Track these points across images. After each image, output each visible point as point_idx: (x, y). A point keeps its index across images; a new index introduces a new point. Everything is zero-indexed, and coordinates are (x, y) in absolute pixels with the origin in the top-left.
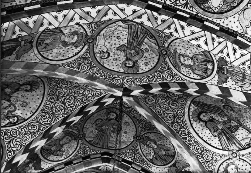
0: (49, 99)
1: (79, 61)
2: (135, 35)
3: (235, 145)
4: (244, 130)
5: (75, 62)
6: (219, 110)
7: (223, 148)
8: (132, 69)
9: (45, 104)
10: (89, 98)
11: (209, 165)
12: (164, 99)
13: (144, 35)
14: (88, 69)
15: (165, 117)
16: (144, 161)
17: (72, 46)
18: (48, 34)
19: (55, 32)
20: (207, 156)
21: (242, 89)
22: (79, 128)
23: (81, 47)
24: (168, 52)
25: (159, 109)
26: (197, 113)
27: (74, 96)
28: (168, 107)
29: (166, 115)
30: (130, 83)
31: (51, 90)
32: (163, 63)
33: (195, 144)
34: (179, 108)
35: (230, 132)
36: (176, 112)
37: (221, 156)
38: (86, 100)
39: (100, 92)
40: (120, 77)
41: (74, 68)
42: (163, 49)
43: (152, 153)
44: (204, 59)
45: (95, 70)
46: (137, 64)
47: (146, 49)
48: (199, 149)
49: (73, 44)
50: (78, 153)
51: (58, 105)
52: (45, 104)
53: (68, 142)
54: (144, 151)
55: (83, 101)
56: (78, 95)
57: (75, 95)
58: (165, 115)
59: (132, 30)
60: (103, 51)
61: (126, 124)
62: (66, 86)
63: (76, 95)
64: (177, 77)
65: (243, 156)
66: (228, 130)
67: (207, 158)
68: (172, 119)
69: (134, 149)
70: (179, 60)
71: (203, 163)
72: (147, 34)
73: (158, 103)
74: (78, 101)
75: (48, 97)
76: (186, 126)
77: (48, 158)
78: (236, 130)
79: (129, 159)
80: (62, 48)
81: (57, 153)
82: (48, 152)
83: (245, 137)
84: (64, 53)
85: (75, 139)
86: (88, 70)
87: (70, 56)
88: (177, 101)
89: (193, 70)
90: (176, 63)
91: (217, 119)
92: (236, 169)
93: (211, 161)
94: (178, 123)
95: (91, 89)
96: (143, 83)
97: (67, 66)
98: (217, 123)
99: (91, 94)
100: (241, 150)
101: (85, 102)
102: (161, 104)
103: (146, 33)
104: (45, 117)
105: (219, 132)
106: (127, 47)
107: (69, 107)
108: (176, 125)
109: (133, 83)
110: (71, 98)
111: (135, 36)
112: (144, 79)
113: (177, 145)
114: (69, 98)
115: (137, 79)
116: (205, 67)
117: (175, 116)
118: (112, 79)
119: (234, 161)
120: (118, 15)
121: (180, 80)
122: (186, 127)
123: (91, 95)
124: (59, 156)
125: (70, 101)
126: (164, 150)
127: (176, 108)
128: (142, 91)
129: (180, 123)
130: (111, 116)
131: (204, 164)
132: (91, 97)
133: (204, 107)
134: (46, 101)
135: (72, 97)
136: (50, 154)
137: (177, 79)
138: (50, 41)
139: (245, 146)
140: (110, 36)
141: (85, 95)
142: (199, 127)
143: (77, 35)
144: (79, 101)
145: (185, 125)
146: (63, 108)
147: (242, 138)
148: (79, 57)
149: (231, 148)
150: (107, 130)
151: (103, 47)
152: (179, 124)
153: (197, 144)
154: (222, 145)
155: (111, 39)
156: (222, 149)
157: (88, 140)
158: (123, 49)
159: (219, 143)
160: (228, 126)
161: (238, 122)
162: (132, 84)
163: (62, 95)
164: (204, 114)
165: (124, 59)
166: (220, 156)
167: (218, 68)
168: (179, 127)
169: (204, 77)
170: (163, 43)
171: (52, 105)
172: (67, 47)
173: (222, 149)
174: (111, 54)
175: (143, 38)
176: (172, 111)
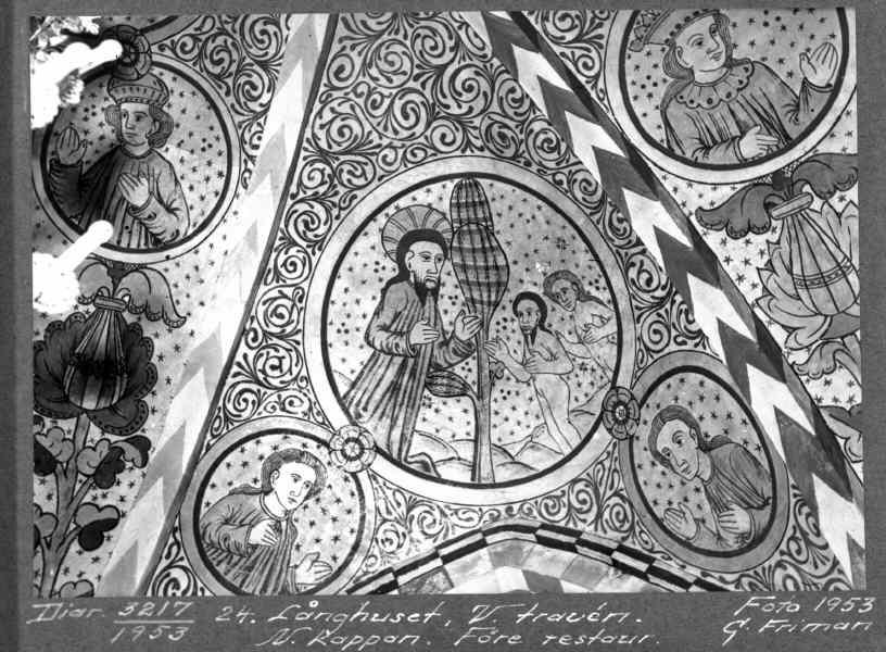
3: (392, 428)
4: (471, 417)
6: (493, 289)
7: (345, 397)
11: (246, 395)
12: (416, 62)
15: (332, 110)
20: (276, 362)
21: (763, 303)
26: (424, 224)
29: (345, 108)
33: (288, 291)
35: (423, 377)
36: (377, 142)
37: (315, 411)
44: (772, 106)
48: (281, 316)
58: (339, 105)
64: (594, 54)
65: (373, 477)
66: (425, 370)
67: (269, 371)
68: (339, 144)
70: (682, 22)
71: (239, 365)
76: (343, 214)
78: (448, 395)
83: (445, 435)
89: (674, 96)
91: (444, 304)
92: (305, 492)
93: (269, 392)
94: (336, 174)
98: (427, 315)
100: (388, 457)
105: (397, 345)
108: (323, 174)
117: (358, 147)
119: (329, 463)
121: (592, 73)
122: (337, 217)
127: (396, 132)
131: (238, 374)
133: (470, 232)
137: (583, 60)
139: (409, 460)
142: (365, 265)
145: (341, 209)
147: (433, 432)
149: (368, 422)
152: (332, 181)
153: (293, 300)
154: (353, 385)
156: (342, 395)
159: (352, 372)
160: (441, 361)
161: (486, 381)
164: (434, 249)
166: (310, 409)
167: (777, 174)
168: (322, 190)
169: (678, 152)
173: (342, 395)
176: (375, 122)
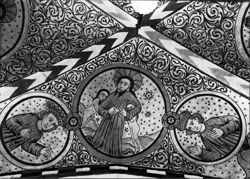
0: (29, 41)
9: (22, 48)
10: (88, 41)
15: (208, 56)
16: (188, 163)
22: (72, 100)
25: (196, 47)
27: (66, 39)
28: (208, 41)
29: (209, 53)
31: (33, 25)
34: (227, 40)
36: (223, 47)
38: (85, 43)
39: (105, 32)
43: (198, 144)
50: (67, 158)
51: (42, 52)
52: (22, 48)
53: (52, 129)
54: (184, 144)
55: (79, 46)
57: (68, 37)
61: (147, 95)
62: (56, 18)
68: (220, 58)
69: (166, 146)
74: (72, 46)
75: (27, 38)
77: (12, 152)
79: (159, 166)
81: (30, 147)
82: (15, 137)
85: (64, 127)
88: (220, 27)
95: (93, 26)
99: (93, 36)
101: (83, 46)
102: (198, 38)
104: (19, 65)
107: (58, 54)
110: (61, 42)
113: (241, 85)
114: (60, 41)
122: (246, 66)
123: (92, 38)
124: (33, 154)
125: (60, 46)
126: (219, 126)
127: (221, 40)
128: (168, 5)
129: (235, 61)
130: (123, 85)
132: (92, 39)
134: (24, 44)
135: (64, 40)
136: (17, 144)
141: (83, 36)
144: (74, 46)
145: (243, 64)
146: (49, 55)
150: (117, 116)
152: (232, 64)
157: (85, 135)
163: (49, 37)
171: (31, 51)
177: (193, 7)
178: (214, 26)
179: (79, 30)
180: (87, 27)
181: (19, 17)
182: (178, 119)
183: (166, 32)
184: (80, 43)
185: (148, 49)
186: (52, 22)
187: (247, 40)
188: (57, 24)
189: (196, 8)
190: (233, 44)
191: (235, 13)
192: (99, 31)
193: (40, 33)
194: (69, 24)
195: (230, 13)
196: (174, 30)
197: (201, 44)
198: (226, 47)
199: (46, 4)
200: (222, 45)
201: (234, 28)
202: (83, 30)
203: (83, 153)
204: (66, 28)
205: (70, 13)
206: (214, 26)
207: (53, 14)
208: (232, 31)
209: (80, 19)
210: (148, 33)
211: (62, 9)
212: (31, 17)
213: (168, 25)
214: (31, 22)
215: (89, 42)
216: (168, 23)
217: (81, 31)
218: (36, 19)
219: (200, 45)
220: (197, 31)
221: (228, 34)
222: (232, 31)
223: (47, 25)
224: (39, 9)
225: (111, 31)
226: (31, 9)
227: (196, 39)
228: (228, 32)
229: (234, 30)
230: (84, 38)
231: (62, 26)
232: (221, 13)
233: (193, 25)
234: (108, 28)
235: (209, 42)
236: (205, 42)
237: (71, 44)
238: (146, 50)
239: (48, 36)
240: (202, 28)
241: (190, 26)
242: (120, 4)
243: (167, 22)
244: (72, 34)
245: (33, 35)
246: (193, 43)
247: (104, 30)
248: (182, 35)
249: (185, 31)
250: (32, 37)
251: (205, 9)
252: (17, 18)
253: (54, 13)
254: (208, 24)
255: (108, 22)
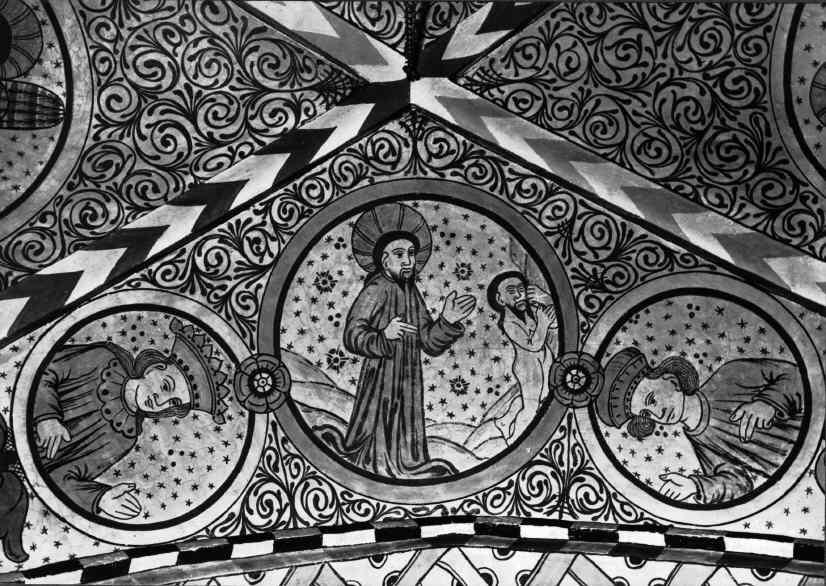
1: (622, 276)
2: (397, 416)
5: (641, 274)
8: (386, 230)
10: (571, 28)
13: (358, 433)
14: (578, 224)
17: (655, 359)
18: (753, 456)
19: (726, 456)
23: (614, 349)
24: (246, 390)
26: (17, 48)
27: (645, 26)
30: (382, 147)
31: (755, 60)
32: (256, 318)
34: (116, 51)
36: (127, 23)
38: (581, 15)
39: (517, 65)
40: (433, 169)
41: (645, 236)
42: (272, 398)
44: (88, 454)
45: (548, 212)
46: (364, 268)
47: (342, 364)
49: (650, 372)
56: (621, 33)
57: (640, 36)
59: (409, 439)
60: (520, 315)
62: (681, 93)
63: (633, 34)
70: (189, 373)
72: (348, 444)
73: (228, 57)
75: (774, 12)
80: (696, 356)
84: (688, 327)
86: (580, 218)
87: (658, 310)
88: (143, 93)
90: (197, 350)
95: (560, 83)
96: (324, 171)
97: (678, 256)
99: (558, 46)
103: (355, 445)
106: (420, 344)
109: (370, 154)
111: (393, 411)
112: (322, 195)
114: (667, 16)
115: (355, 183)
116: (70, 415)
118: (465, 157)
120: (477, 570)
123: (558, 41)
127: (133, 48)
132: (560, 35)
135: (651, 22)
138: (746, 408)
140: (497, 394)
141: (590, 43)
143: (634, 417)
148: (623, 293)
151: (521, 340)
155: (489, 379)
158: (437, 332)
162: (373, 145)
163: (703, 28)
165: (423, 275)
169: (58, 356)
170: (275, 430)
172: (673, 358)
174: (481, 298)
175: (359, 419)
177: (234, 153)
178: (160, 96)
179: (605, 65)
180: (578, 76)
181: (802, 80)
182: (244, 401)
183: (316, 76)
184: (599, 17)
185: (373, 22)
186: (695, 80)
187: (49, 50)
188: (676, 75)
189: (224, 150)
190: (94, 37)
191: (96, 137)
192: (537, 68)
193: (732, 34)
194: (638, 81)
195: (112, 138)
196: (292, 85)
197: (197, 35)
198: (115, 24)
199: (715, 131)
200: (129, 29)
201: (96, 93)
202: (590, 65)
203: (583, 480)
204: (645, 64)
205: (635, 113)
206: (160, 96)
207: (691, 104)
208: (99, 80)
209: (602, 98)
210: (378, 60)
211: (664, 124)
212: (763, 84)
213: (312, 99)
214: (762, 68)
215: (570, 24)
216: (314, 107)
217: (597, 60)
218: (748, 80)
219: (202, 29)
220: (216, 82)
221: (115, 72)
222: (99, 80)
223: (711, 66)
224: (739, 113)
225: (499, 72)
226: (765, 109)
227: (216, 54)
228: (115, 77)
229: (95, 84)
230: (587, 34)
231: (660, 70)
232: (143, 138)
233: (231, 103)
234: (508, 82)
235: (175, 40)
236: (186, 40)
237: (628, 10)
238: (380, 18)
239: (704, 32)
240: (200, 93)
241: (238, 98)
242: (473, 161)
243: (318, 108)
244: (625, 48)
245: (756, 27)
246: (227, 40)
247: (520, 71)
248: (265, 66)
249: (255, 82)
250: (758, 17)
251: (195, 148)
252: (809, 74)
253: (687, 109)
254: (184, 106)
255: (511, 100)
